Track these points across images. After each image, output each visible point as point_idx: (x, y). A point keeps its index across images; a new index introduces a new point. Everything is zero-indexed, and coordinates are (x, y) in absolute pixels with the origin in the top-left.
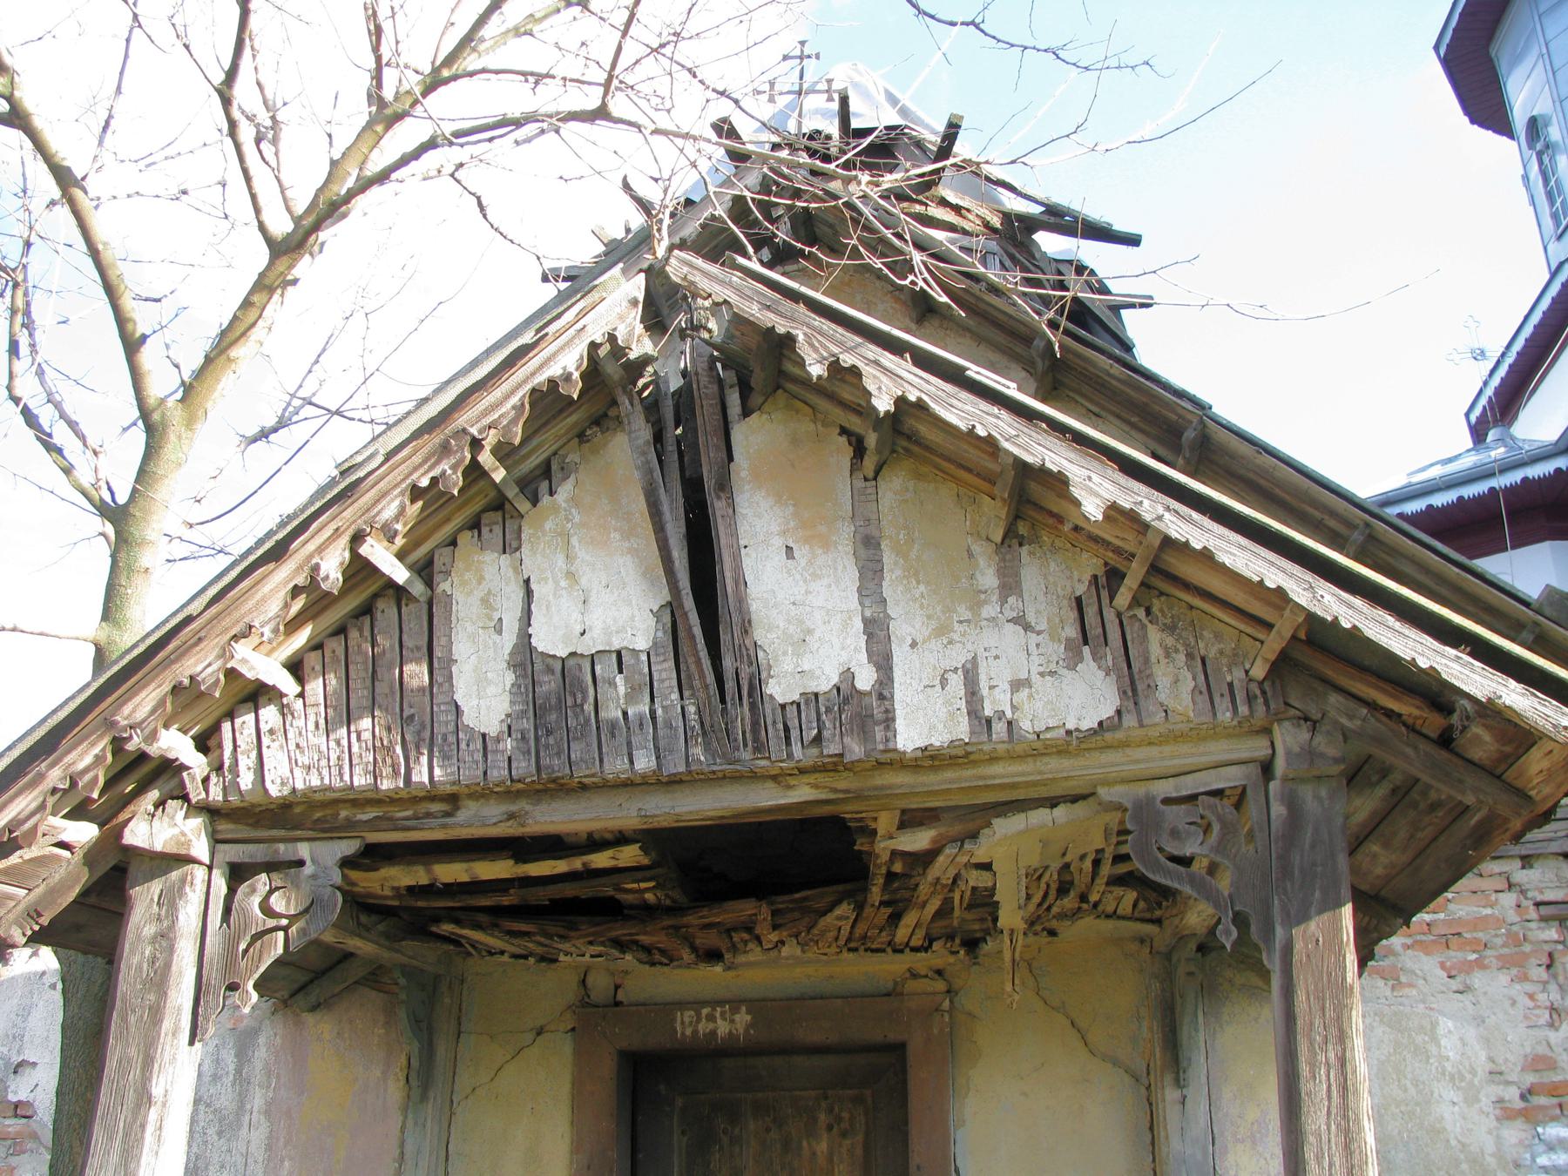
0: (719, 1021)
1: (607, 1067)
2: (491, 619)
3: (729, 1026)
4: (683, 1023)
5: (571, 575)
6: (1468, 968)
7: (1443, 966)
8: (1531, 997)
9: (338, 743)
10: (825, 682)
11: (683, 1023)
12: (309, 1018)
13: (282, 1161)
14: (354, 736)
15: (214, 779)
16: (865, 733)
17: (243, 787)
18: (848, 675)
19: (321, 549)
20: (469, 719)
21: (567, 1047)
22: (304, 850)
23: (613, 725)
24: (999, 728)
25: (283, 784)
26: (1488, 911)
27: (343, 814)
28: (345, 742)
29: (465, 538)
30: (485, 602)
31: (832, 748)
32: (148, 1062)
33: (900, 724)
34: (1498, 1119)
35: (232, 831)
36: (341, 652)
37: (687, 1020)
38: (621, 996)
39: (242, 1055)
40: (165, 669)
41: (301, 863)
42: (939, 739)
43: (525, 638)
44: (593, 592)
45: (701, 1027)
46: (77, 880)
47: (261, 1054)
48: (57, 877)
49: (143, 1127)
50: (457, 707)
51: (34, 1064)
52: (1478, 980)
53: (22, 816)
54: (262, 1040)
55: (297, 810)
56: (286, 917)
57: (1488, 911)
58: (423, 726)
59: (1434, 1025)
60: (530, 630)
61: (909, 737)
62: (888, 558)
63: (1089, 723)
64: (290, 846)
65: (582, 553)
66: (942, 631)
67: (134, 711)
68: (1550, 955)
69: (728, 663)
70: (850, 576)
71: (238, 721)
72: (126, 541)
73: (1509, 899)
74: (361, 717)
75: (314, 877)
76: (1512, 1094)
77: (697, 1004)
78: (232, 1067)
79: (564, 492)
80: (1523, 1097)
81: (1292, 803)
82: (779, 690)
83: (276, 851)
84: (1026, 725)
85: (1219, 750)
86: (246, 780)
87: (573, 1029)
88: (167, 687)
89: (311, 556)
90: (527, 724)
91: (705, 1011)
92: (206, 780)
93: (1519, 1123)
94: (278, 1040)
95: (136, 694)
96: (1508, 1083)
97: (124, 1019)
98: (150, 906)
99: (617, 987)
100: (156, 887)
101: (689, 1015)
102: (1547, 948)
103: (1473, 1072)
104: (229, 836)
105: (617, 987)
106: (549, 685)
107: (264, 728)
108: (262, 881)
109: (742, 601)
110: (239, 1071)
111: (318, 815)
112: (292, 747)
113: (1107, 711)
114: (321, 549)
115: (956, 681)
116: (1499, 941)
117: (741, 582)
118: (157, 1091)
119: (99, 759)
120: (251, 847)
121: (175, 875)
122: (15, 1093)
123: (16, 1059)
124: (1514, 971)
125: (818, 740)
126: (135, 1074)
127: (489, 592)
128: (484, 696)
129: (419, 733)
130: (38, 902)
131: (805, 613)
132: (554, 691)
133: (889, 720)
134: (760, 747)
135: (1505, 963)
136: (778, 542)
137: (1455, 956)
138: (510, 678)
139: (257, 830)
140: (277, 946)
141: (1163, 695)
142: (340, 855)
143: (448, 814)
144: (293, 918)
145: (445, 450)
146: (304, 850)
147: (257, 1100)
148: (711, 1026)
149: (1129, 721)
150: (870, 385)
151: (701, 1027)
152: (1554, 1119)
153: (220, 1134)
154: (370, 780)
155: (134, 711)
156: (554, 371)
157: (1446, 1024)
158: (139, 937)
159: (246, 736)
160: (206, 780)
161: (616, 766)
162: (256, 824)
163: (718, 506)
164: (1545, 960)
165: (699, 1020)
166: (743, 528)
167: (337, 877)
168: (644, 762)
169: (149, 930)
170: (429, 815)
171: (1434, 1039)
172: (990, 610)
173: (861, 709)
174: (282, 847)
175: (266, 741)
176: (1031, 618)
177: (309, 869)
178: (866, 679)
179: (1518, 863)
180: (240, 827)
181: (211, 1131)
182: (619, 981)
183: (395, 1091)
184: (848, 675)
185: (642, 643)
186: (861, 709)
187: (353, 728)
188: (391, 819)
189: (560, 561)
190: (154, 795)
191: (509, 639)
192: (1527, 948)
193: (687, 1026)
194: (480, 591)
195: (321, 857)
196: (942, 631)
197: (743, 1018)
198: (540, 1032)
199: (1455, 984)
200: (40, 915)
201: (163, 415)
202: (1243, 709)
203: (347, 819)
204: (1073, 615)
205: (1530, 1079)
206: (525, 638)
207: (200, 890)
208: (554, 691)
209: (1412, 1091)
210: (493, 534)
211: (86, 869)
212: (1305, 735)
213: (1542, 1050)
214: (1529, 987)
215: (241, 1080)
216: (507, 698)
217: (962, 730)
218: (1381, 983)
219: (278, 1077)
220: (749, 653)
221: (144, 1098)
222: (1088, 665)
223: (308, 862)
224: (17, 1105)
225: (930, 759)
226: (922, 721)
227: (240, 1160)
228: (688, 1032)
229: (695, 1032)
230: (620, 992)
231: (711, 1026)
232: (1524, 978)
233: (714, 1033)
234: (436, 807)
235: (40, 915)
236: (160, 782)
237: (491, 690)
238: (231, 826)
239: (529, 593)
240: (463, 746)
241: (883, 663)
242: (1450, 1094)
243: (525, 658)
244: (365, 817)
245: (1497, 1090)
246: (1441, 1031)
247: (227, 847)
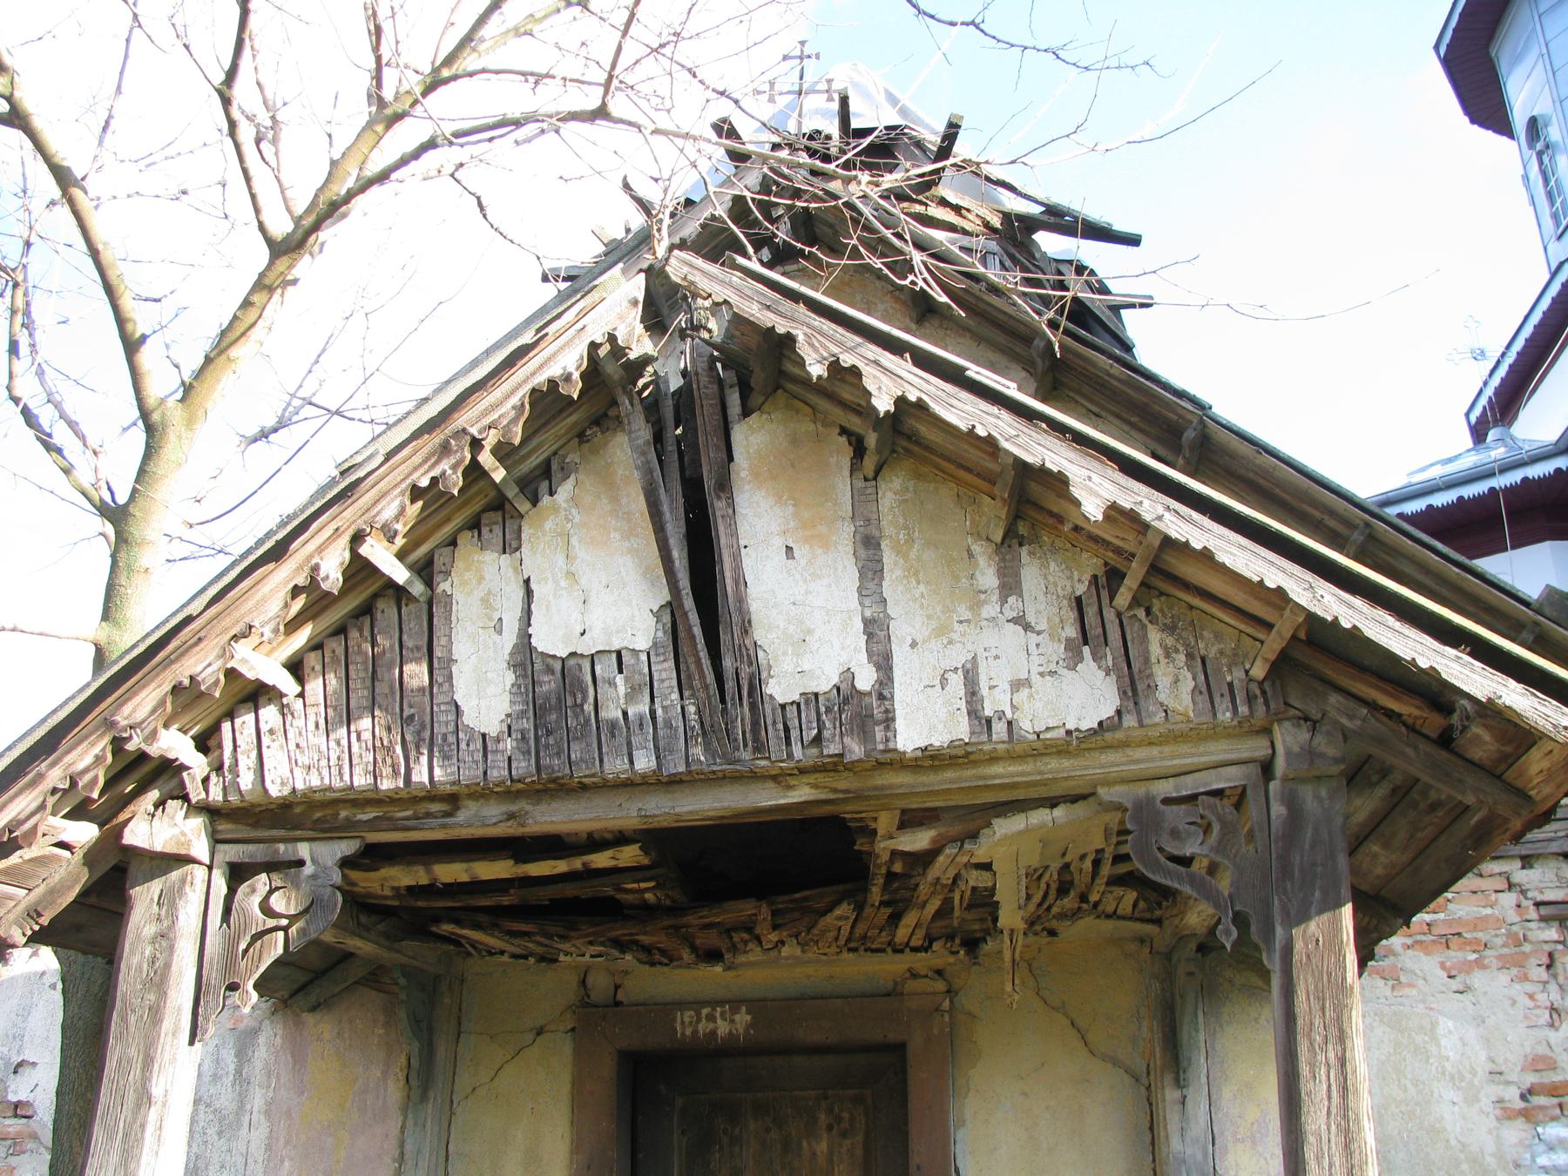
0: (719, 1021)
1: (607, 1067)
2: (490, 619)
3: (728, 1026)
4: (683, 1023)
5: (571, 575)
6: (1468, 968)
7: (1443, 966)
8: (1531, 997)
9: (338, 743)
10: (824, 682)
11: (683, 1023)
12: (309, 1018)
13: (282, 1161)
14: (354, 736)
15: (214, 778)
16: (865, 735)
17: (243, 788)
18: (848, 675)
19: (321, 549)
20: (468, 719)
21: (567, 1048)
22: (304, 850)
23: (613, 725)
24: (999, 729)
25: (283, 784)
26: (1488, 911)
27: (343, 814)
28: (345, 742)
29: (465, 539)
30: (485, 602)
31: (832, 749)
32: (148, 1062)
33: (900, 724)
34: (1498, 1119)
35: (231, 831)
36: (340, 651)
37: (687, 1020)
38: (621, 996)
39: (242, 1055)
40: (165, 668)
41: (301, 863)
42: (939, 739)
43: (525, 637)
44: (591, 586)
45: (701, 1027)
46: (76, 881)
47: (262, 1053)
48: (57, 877)
49: (143, 1126)
50: (457, 707)
51: (34, 1064)
52: (1478, 979)
53: (22, 816)
54: (262, 1040)
55: (298, 810)
56: (286, 917)
57: (1488, 911)
58: (423, 726)
59: (1434, 1025)
60: (530, 630)
61: (909, 737)
62: (888, 557)
63: (1089, 723)
64: (290, 846)
65: (582, 552)
66: (941, 631)
67: (134, 711)
68: (1550, 955)
69: (728, 663)
70: (851, 576)
71: (238, 721)
72: (126, 541)
73: (1509, 899)
74: (360, 717)
75: (314, 877)
76: (1512, 1094)
77: (697, 1004)
78: (232, 1067)
79: (565, 491)
80: (1523, 1097)
81: (1292, 803)
82: (780, 689)
83: (277, 851)
84: (1026, 725)
85: (1218, 750)
86: (246, 780)
87: (573, 1029)
88: (167, 687)
89: (311, 556)
90: (527, 724)
91: (705, 1011)
92: (206, 780)
93: (1520, 1123)
94: (279, 1040)
95: (136, 694)
96: (1508, 1083)
97: (124, 1019)
98: (150, 907)
99: (617, 987)
100: (156, 886)
101: (689, 1015)
102: (1548, 948)
103: (1473, 1072)
104: (229, 836)
105: (617, 987)
106: (548, 685)
107: (264, 728)
108: (262, 881)
109: (741, 600)
110: (239, 1072)
111: (318, 815)
112: (292, 747)
113: (1107, 710)
114: (321, 549)
115: (956, 681)
116: (1499, 941)
117: (740, 581)
118: (157, 1090)
119: (99, 759)
120: (251, 847)
121: (175, 875)
122: (15, 1093)
123: (16, 1059)
124: (1514, 971)
125: (818, 740)
126: (136, 1072)
127: (489, 592)
128: (484, 696)
129: (419, 733)
130: (38, 902)
131: (805, 609)
132: (554, 691)
133: (889, 720)
134: (759, 747)
135: (1505, 964)
136: (778, 543)
137: (1455, 956)
138: (510, 678)
139: (257, 830)
140: (276, 947)
141: (1163, 695)
142: (339, 856)
143: (448, 814)
144: (293, 919)
145: (445, 450)
146: (304, 850)
147: (258, 1100)
148: (711, 1026)
149: (1130, 721)
150: (869, 383)
151: (701, 1027)
152: (1553, 1119)
153: (220, 1133)
154: (370, 780)
155: (134, 711)
156: (554, 371)
157: (1445, 1024)
158: (138, 936)
159: (246, 736)
160: (206, 780)
161: (615, 766)
162: (256, 825)
163: (718, 506)
164: (1545, 960)
165: (699, 1020)
166: (743, 528)
167: (337, 877)
168: (644, 762)
169: (150, 930)
170: (428, 815)
171: (1434, 1038)
172: (991, 610)
173: (861, 709)
174: (282, 847)
175: (266, 740)
176: (1031, 618)
177: (309, 869)
178: (866, 679)
179: (1518, 864)
180: (240, 827)
181: (212, 1131)
182: (619, 981)
183: (394, 1091)
184: (848, 675)
185: (642, 643)
186: (861, 709)
187: (353, 728)
188: (390, 819)
189: (560, 560)
190: (154, 795)
191: (510, 638)
192: (1527, 948)
193: (686, 1025)
194: (479, 588)
195: (320, 856)
196: (941, 631)
197: (743, 1018)
198: (540, 1032)
199: (1455, 984)
200: (40, 915)
201: (164, 415)
202: (1243, 709)
203: (347, 818)
204: (1072, 615)
205: (1530, 1079)
206: (525, 637)
207: (199, 889)
208: (554, 691)
209: (1412, 1091)
210: (493, 535)
211: (86, 870)
212: (1305, 735)
213: (1542, 1050)
214: (1529, 987)
215: (240, 1078)
216: (507, 697)
217: (962, 730)
218: (1381, 983)
219: (278, 1078)
220: (749, 655)
221: (144, 1098)
222: (1088, 665)
223: (308, 863)
224: (17, 1105)
225: (931, 759)
226: (923, 721)
227: (241, 1160)
228: (688, 1032)
229: (695, 1032)
230: (620, 992)
231: (711, 1026)
232: (1525, 978)
233: (714, 1033)
234: (436, 807)
235: (40, 915)
236: (160, 782)
237: (492, 690)
238: (230, 826)
239: (529, 593)
240: (463, 746)
241: (884, 664)
242: (1450, 1094)
243: (525, 657)
244: (364, 817)
245: (1496, 1091)
246: (1440, 1030)
247: (226, 847)
